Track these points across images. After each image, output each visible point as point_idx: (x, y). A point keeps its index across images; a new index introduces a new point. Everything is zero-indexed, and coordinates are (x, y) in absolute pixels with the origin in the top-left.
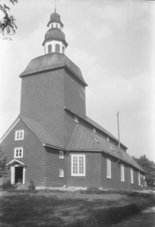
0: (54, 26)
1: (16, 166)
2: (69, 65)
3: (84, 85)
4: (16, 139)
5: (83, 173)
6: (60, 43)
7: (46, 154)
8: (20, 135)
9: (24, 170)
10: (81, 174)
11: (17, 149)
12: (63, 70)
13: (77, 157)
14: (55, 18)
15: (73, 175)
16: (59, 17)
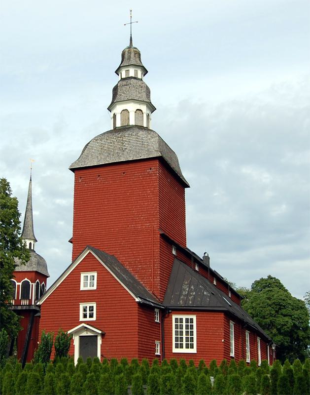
1: (84, 334)
2: (167, 158)
3: (185, 185)
4: (82, 288)
5: (192, 347)
6: (144, 108)
7: (141, 313)
8: (88, 282)
9: (99, 341)
10: (179, 349)
11: (85, 305)
12: (157, 162)
13: (181, 319)
14: (131, 57)
15: (175, 350)
16: (138, 54)
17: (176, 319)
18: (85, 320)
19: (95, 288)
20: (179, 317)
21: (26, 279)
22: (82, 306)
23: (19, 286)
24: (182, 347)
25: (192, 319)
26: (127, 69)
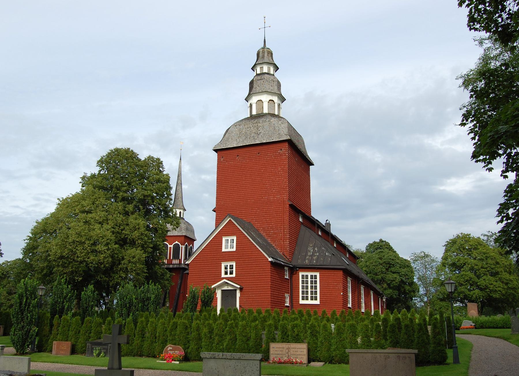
0: (265, 70)
1: (226, 288)
2: (295, 141)
4: (224, 250)
5: (316, 299)
8: (229, 244)
9: (238, 294)
12: (287, 144)
13: (307, 276)
14: (264, 56)
15: (301, 302)
16: (271, 54)
17: (303, 276)
18: (226, 276)
19: (234, 249)
20: (305, 274)
21: (177, 242)
22: (223, 265)
23: (170, 248)
24: (307, 299)
25: (316, 276)
26: (261, 66)
